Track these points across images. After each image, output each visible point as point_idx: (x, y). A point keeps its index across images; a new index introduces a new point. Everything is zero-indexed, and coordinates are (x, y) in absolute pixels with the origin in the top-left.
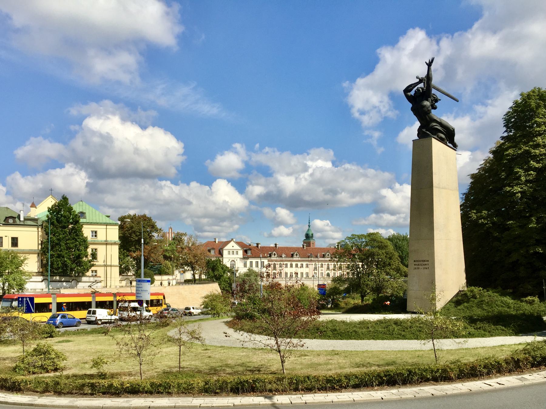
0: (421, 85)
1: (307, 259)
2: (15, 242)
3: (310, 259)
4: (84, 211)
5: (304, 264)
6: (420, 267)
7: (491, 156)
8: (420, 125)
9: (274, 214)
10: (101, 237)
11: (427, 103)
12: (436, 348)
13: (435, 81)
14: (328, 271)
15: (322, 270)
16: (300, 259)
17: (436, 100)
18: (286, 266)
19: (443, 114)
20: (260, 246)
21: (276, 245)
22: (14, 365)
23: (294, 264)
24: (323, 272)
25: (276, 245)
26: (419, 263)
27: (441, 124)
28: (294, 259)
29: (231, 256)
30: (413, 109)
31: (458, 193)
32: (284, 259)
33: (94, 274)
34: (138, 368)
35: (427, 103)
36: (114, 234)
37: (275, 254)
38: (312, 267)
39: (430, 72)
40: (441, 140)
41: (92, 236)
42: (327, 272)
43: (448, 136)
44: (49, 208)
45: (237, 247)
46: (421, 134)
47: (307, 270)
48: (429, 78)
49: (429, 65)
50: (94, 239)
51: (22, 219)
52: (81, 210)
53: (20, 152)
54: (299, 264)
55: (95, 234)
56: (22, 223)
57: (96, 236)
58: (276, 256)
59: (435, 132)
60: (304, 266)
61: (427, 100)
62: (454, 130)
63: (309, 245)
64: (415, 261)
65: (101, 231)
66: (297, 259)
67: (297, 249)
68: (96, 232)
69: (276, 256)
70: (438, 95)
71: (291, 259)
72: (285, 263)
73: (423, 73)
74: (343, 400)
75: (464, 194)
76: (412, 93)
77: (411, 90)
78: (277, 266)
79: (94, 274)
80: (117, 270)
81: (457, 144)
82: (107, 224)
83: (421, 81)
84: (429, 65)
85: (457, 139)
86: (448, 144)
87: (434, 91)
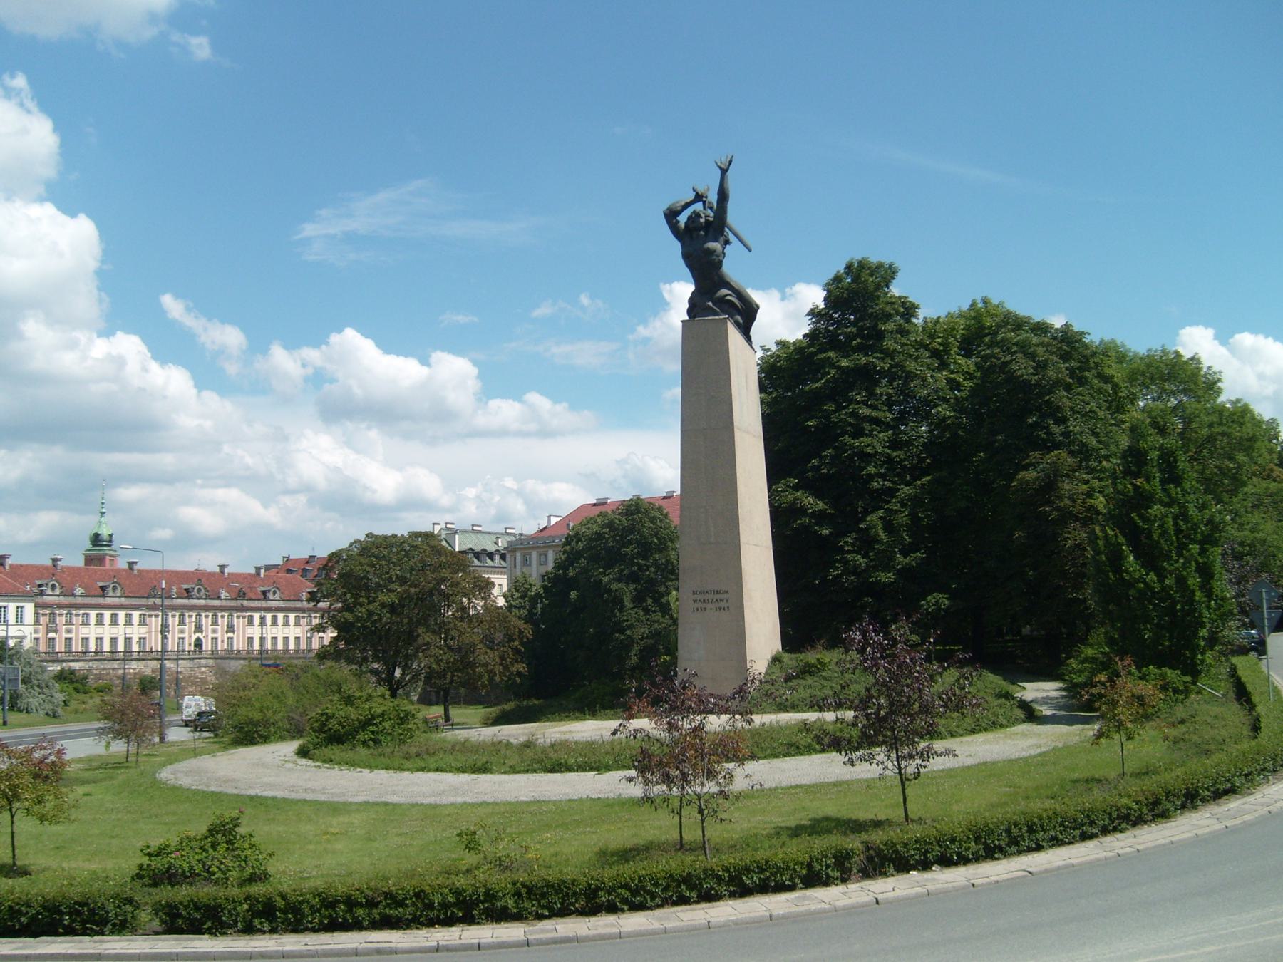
0: (698, 206)
1: (143, 601)
3: (151, 601)
6: (709, 606)
12: (677, 818)
14: (198, 635)
15: (214, 631)
17: (727, 242)
18: (85, 623)
20: (227, 571)
24: (186, 635)
25: (55, 561)
26: (706, 597)
28: (109, 601)
32: (79, 600)
34: (676, 836)
38: (155, 622)
40: (737, 324)
42: (194, 637)
44: (887, 274)
46: (696, 307)
47: (84, 631)
49: (724, 172)
58: (58, 591)
63: (100, 560)
64: (694, 593)
66: (116, 601)
69: (58, 591)
70: (732, 237)
71: (101, 601)
74: (1151, 845)
76: (682, 219)
84: (724, 172)
85: (751, 333)
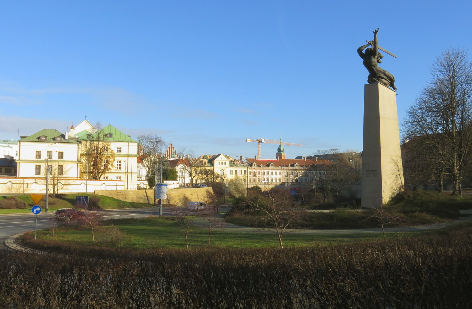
2: (61, 155)
4: (112, 133)
5: (278, 172)
8: (369, 74)
9: (212, 168)
10: (124, 151)
13: (378, 46)
16: (274, 168)
21: (255, 157)
22: (395, 176)
23: (270, 171)
28: (270, 168)
29: (221, 166)
31: (397, 122)
33: (118, 179)
36: (133, 149)
37: (255, 165)
41: (118, 151)
45: (225, 159)
47: (280, 176)
50: (119, 153)
51: (66, 138)
52: (109, 132)
54: (274, 171)
55: (120, 150)
56: (66, 141)
57: (120, 151)
60: (278, 173)
65: (124, 146)
66: (272, 168)
67: (273, 161)
68: (120, 148)
71: (268, 168)
72: (263, 171)
73: (371, 39)
76: (364, 52)
78: (257, 174)
79: (118, 179)
80: (135, 159)
82: (128, 142)
83: (369, 44)
84: (375, 33)
85: (396, 85)
86: (390, 87)
87: (378, 51)
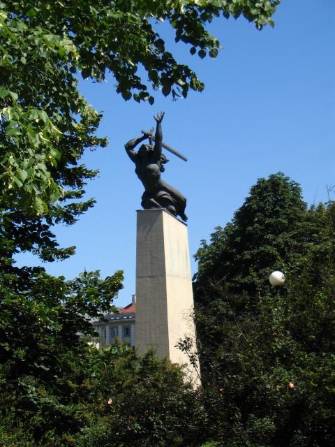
0: (146, 142)
7: (121, 94)
11: (154, 166)
13: (165, 141)
17: (165, 161)
19: (172, 177)
27: (172, 194)
30: (137, 171)
35: (154, 166)
39: (160, 131)
40: (172, 213)
43: (178, 207)
48: (158, 138)
49: (159, 122)
53: (30, 192)
59: (165, 203)
61: (156, 163)
62: (186, 201)
73: (150, 127)
75: (91, 207)
76: (136, 150)
77: (134, 146)
81: (187, 216)
83: (146, 136)
84: (159, 122)
85: (187, 212)
87: (164, 151)
